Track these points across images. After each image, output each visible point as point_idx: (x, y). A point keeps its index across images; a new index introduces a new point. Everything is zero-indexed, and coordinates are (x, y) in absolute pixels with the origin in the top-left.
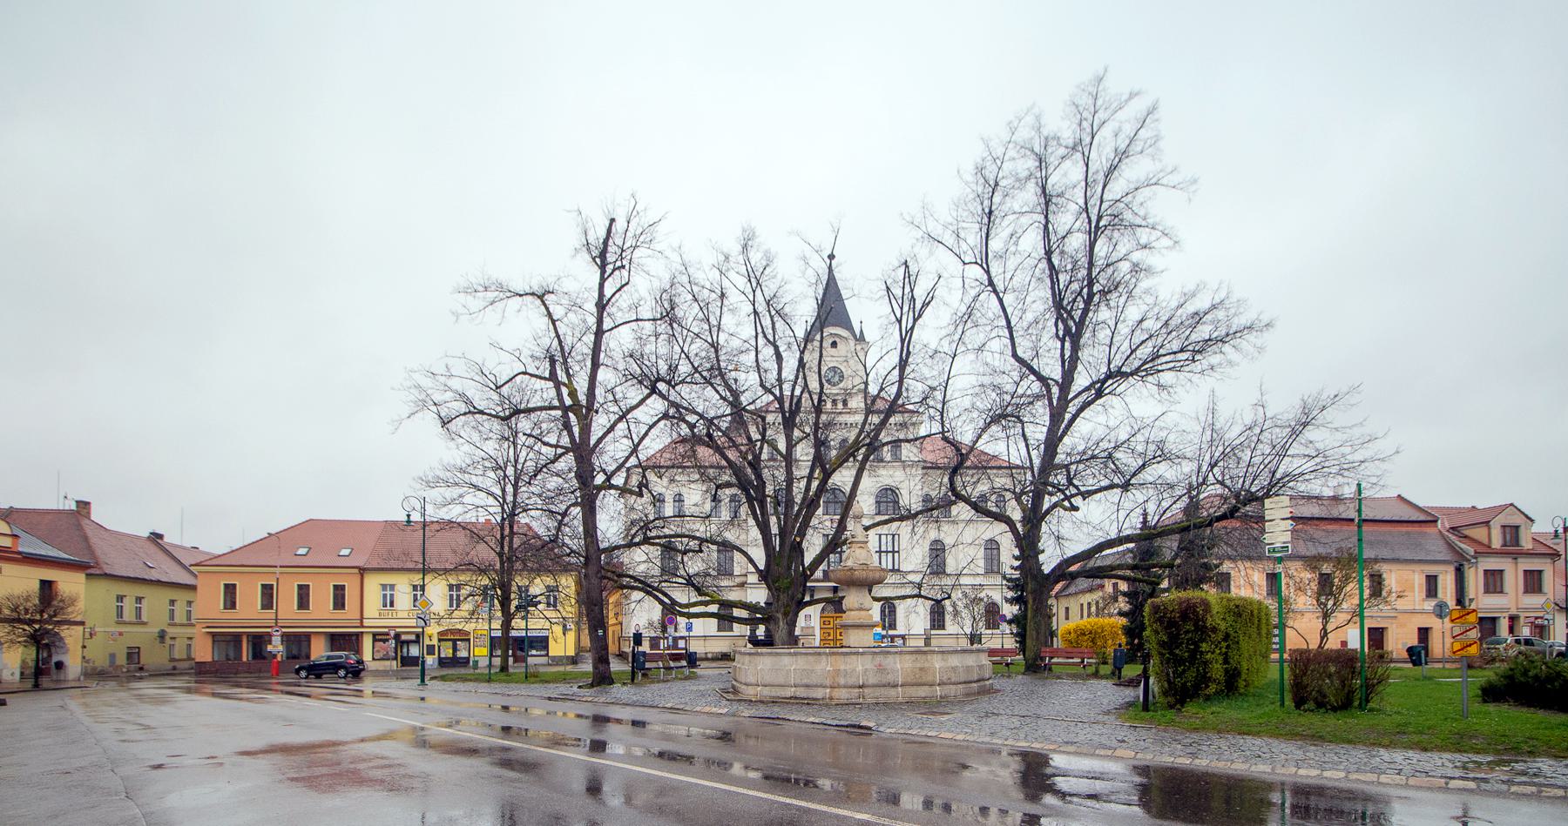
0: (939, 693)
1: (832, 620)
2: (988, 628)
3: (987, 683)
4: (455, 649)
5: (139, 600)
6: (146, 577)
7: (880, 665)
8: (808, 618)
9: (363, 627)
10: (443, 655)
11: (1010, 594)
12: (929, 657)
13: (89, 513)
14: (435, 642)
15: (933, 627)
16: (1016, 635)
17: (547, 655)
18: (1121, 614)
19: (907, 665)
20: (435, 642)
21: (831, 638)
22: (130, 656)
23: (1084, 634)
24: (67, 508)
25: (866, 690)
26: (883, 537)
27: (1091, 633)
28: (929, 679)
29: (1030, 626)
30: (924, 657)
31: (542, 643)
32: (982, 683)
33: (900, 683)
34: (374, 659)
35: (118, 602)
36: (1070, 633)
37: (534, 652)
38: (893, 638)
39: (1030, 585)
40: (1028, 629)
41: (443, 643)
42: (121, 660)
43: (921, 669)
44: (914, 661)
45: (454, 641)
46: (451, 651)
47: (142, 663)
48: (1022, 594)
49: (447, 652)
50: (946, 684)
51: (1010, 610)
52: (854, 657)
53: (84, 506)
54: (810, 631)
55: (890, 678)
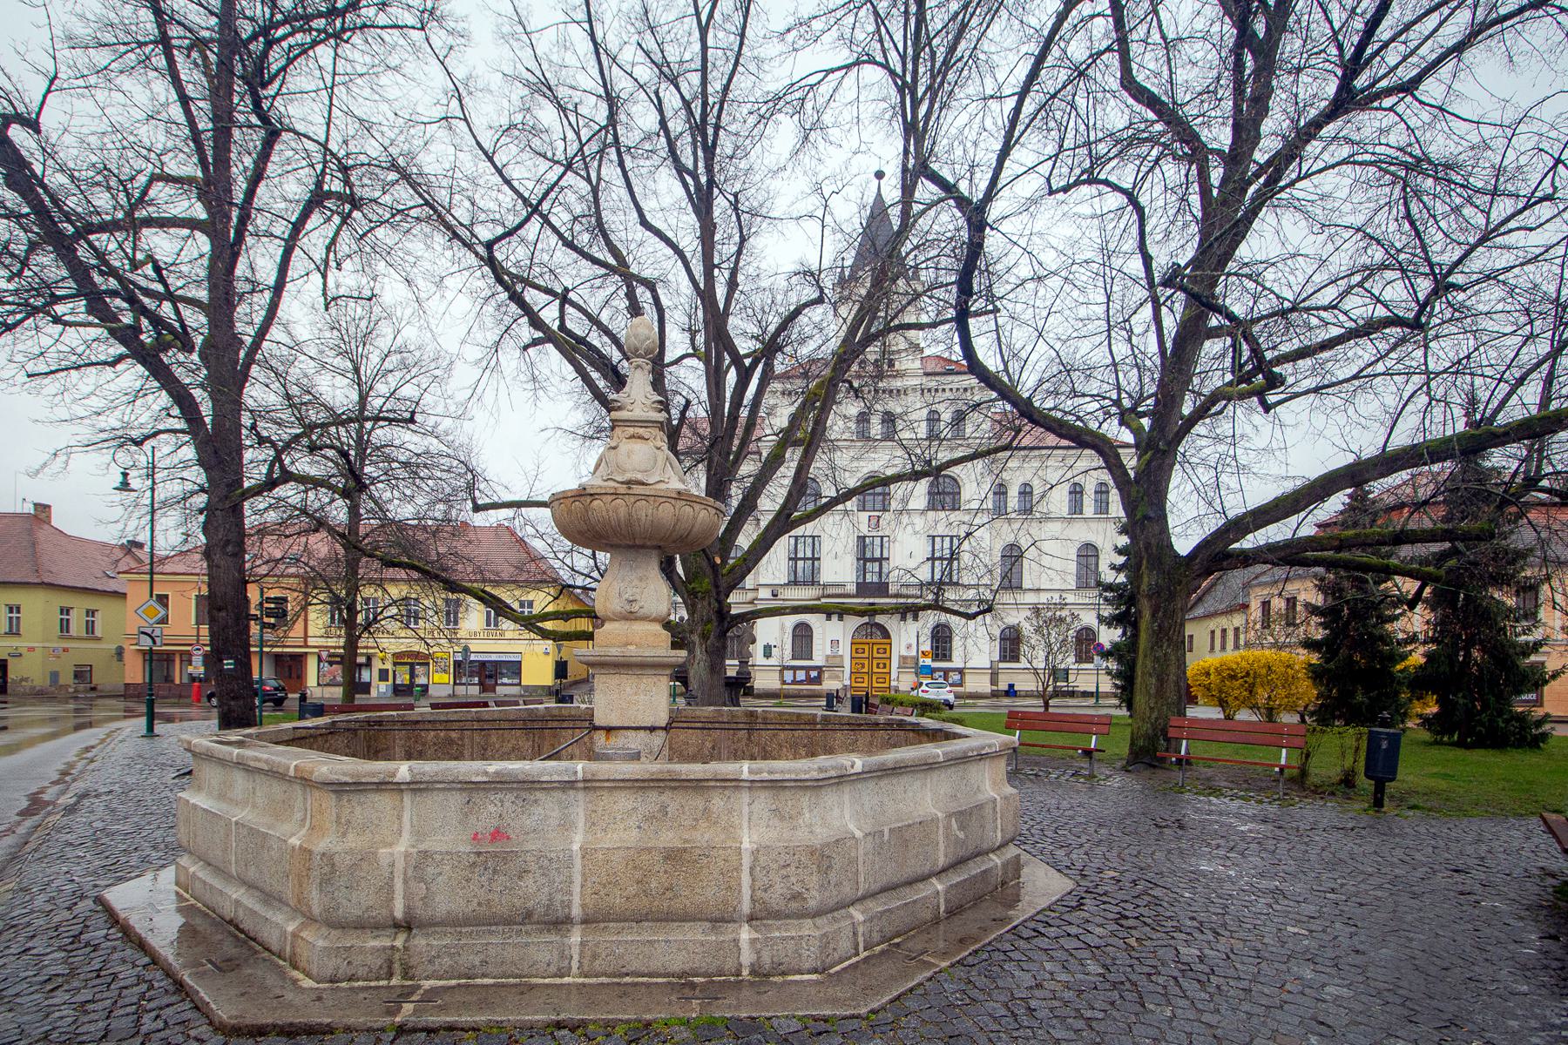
0: (747, 957)
1: (866, 647)
2: (1079, 660)
3: (996, 860)
4: (413, 675)
5: (91, 613)
6: (99, 588)
7: (497, 835)
8: (835, 644)
9: (307, 647)
10: (398, 682)
11: (1107, 611)
12: (717, 802)
13: (49, 517)
14: (389, 666)
15: (1003, 659)
16: (1118, 675)
17: (520, 684)
18: (1310, 645)
19: (611, 839)
20: (389, 666)
21: (865, 670)
22: (77, 675)
23: (1233, 677)
24: (26, 511)
25: (420, 942)
26: (938, 540)
27: (1248, 674)
28: (708, 894)
29: (1143, 665)
30: (697, 802)
31: (515, 668)
32: (975, 868)
33: (576, 911)
34: (319, 685)
35: (62, 613)
36: (1208, 674)
37: (505, 680)
38: (946, 672)
39: (1146, 579)
40: (1139, 672)
41: (399, 668)
42: (67, 678)
43: (673, 856)
44: (650, 818)
45: (412, 666)
46: (408, 677)
47: (94, 682)
48: (1128, 609)
49: (403, 678)
50: (777, 915)
51: (1109, 636)
52: (384, 801)
53: (43, 510)
54: (837, 661)
55: (533, 891)
